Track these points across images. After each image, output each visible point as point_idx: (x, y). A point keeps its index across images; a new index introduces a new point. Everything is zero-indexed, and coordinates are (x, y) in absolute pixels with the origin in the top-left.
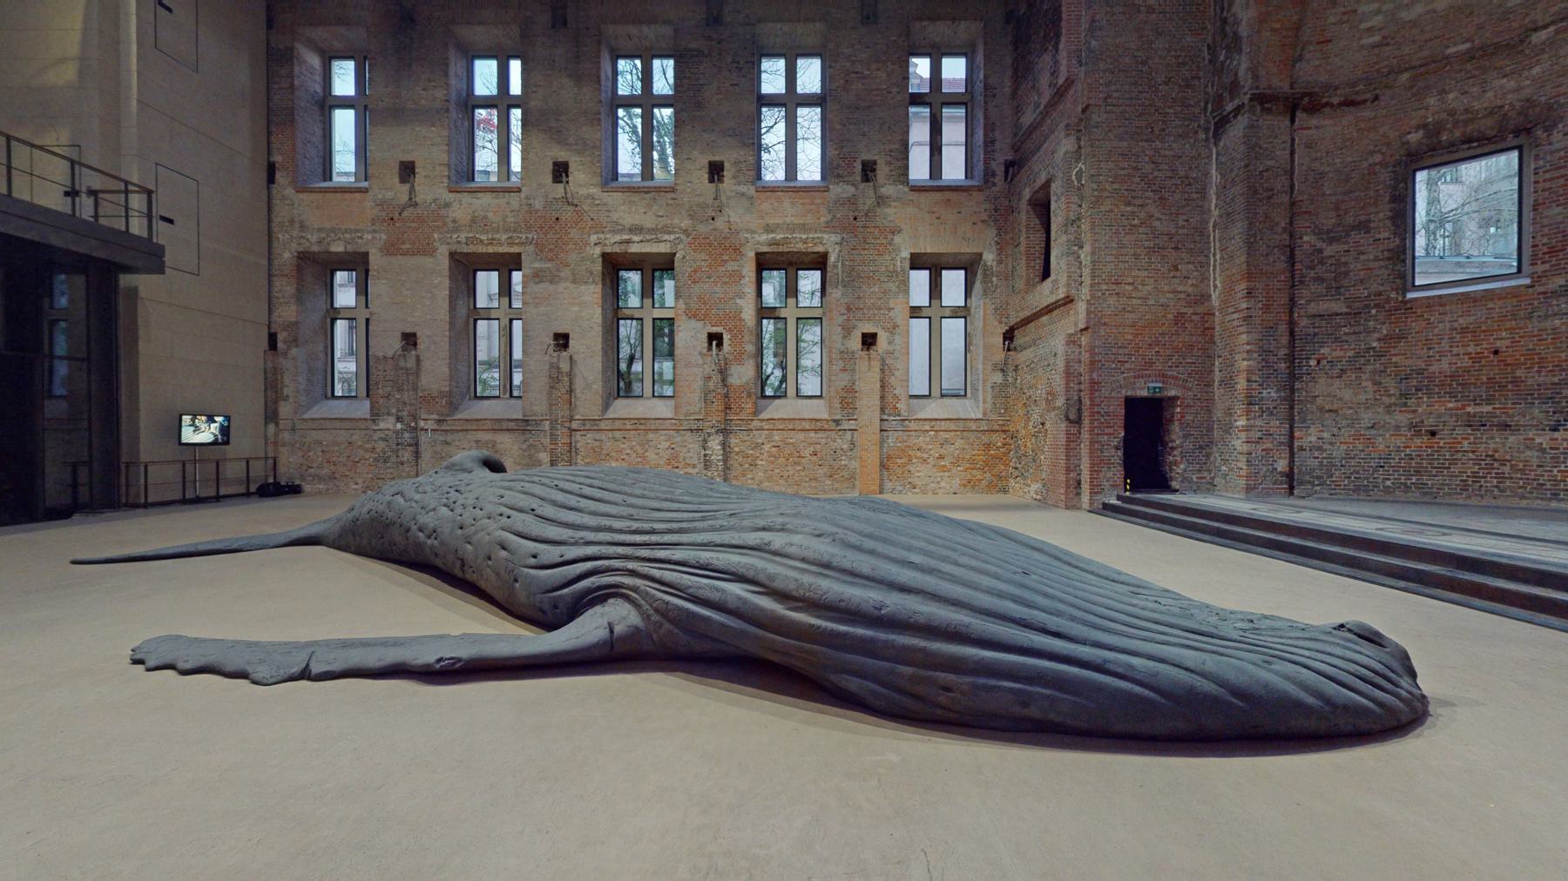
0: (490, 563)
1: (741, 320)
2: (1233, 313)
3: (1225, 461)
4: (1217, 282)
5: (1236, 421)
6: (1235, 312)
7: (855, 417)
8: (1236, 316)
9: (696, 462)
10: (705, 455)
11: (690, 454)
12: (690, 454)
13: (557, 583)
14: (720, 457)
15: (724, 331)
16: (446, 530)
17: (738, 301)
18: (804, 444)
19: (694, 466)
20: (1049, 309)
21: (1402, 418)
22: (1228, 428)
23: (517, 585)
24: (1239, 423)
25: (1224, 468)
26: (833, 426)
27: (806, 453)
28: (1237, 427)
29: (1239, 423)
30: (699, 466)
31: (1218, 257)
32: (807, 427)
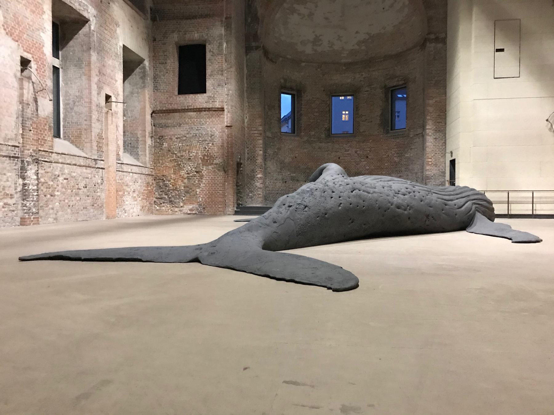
0: (443, 212)
1: (43, 53)
2: (254, 130)
3: (251, 192)
4: (247, 116)
5: (256, 175)
6: (256, 130)
7: (103, 159)
8: (256, 132)
9: (12, 191)
10: (24, 185)
11: (8, 184)
12: (8, 184)
13: (467, 213)
14: (428, 168)
15: (32, 59)
16: (414, 203)
17: (42, 34)
18: (81, 177)
19: (12, 196)
20: (200, 110)
21: (280, 177)
22: (252, 178)
23: (457, 216)
24: (259, 176)
25: (250, 194)
26: (92, 164)
27: (81, 185)
28: (258, 178)
29: (259, 176)
30: (16, 196)
31: (247, 105)
32: (82, 164)
